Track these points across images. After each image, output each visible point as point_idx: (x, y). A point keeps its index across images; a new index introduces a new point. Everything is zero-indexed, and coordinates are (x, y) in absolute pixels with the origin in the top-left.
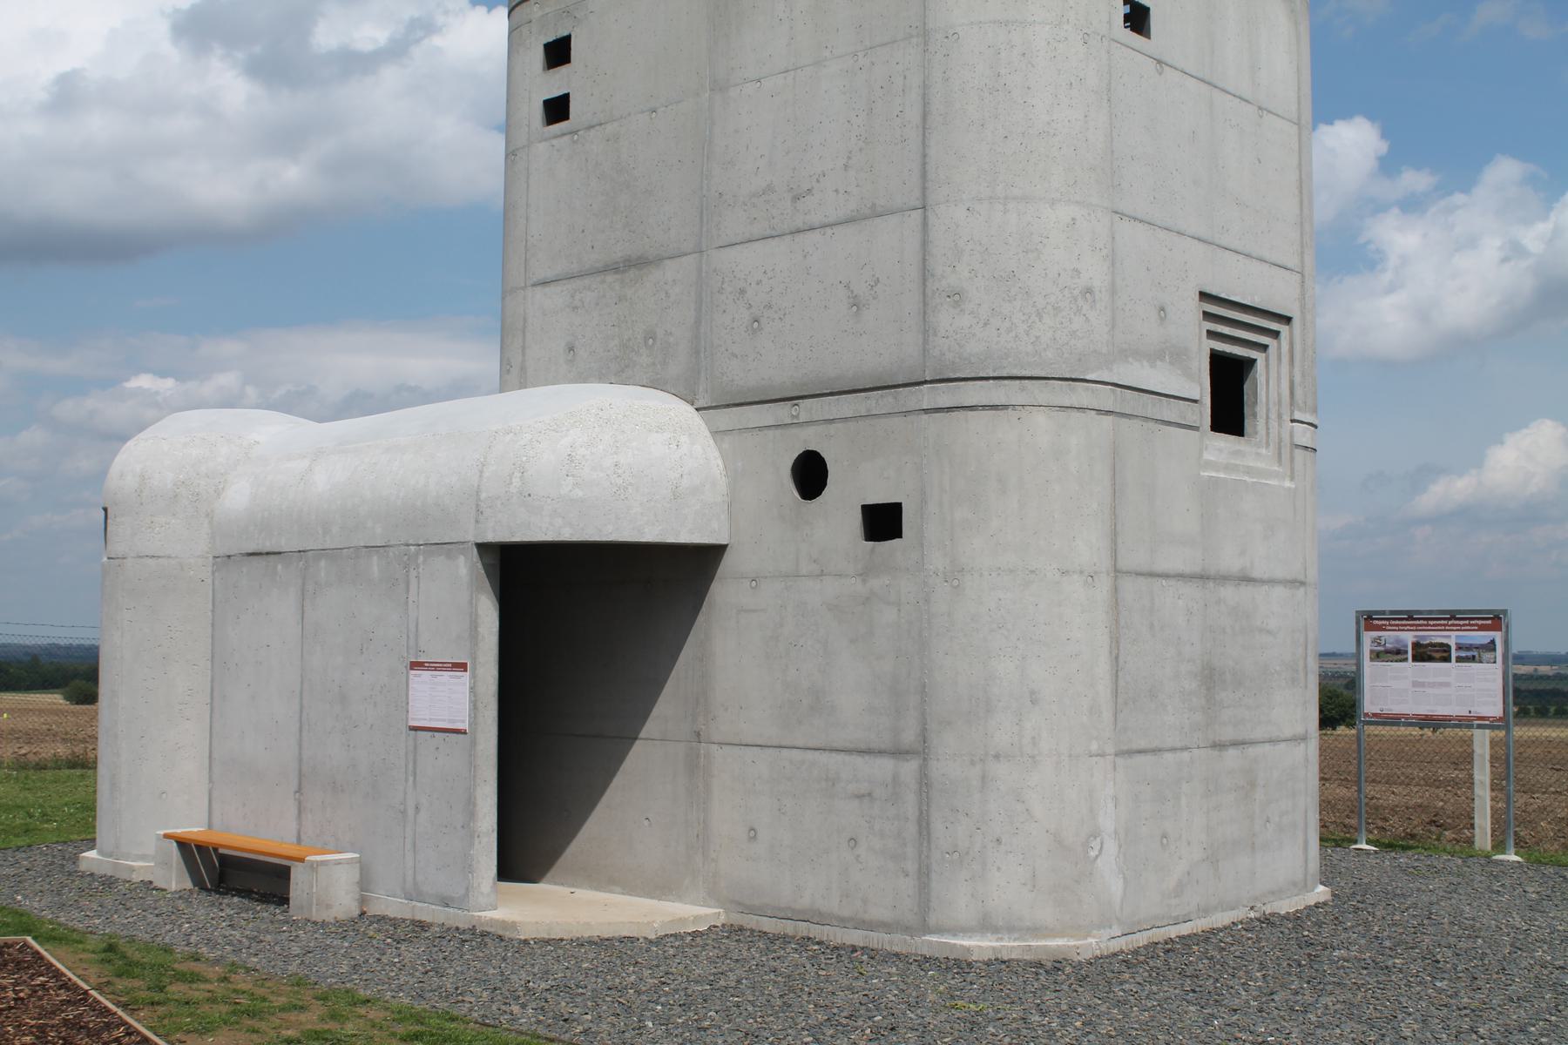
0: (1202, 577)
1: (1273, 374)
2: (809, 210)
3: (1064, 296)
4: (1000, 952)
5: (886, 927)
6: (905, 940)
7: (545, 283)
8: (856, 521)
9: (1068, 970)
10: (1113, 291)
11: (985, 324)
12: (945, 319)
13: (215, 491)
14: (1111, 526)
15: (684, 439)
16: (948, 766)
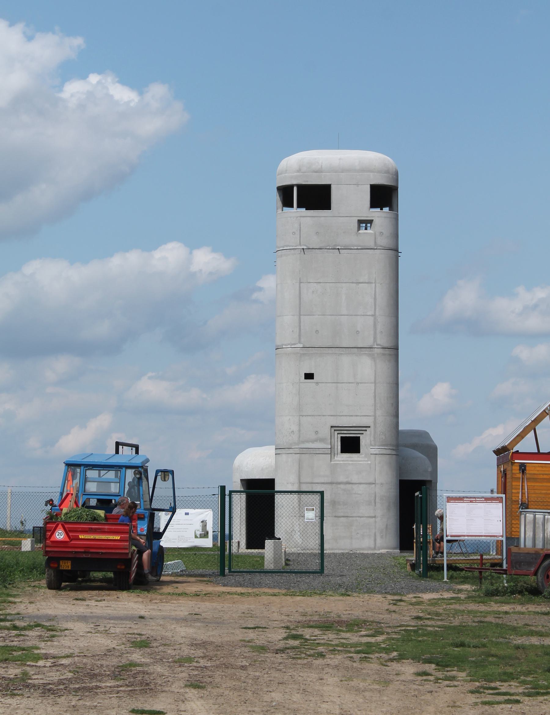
0: (331, 483)
10: (299, 431)
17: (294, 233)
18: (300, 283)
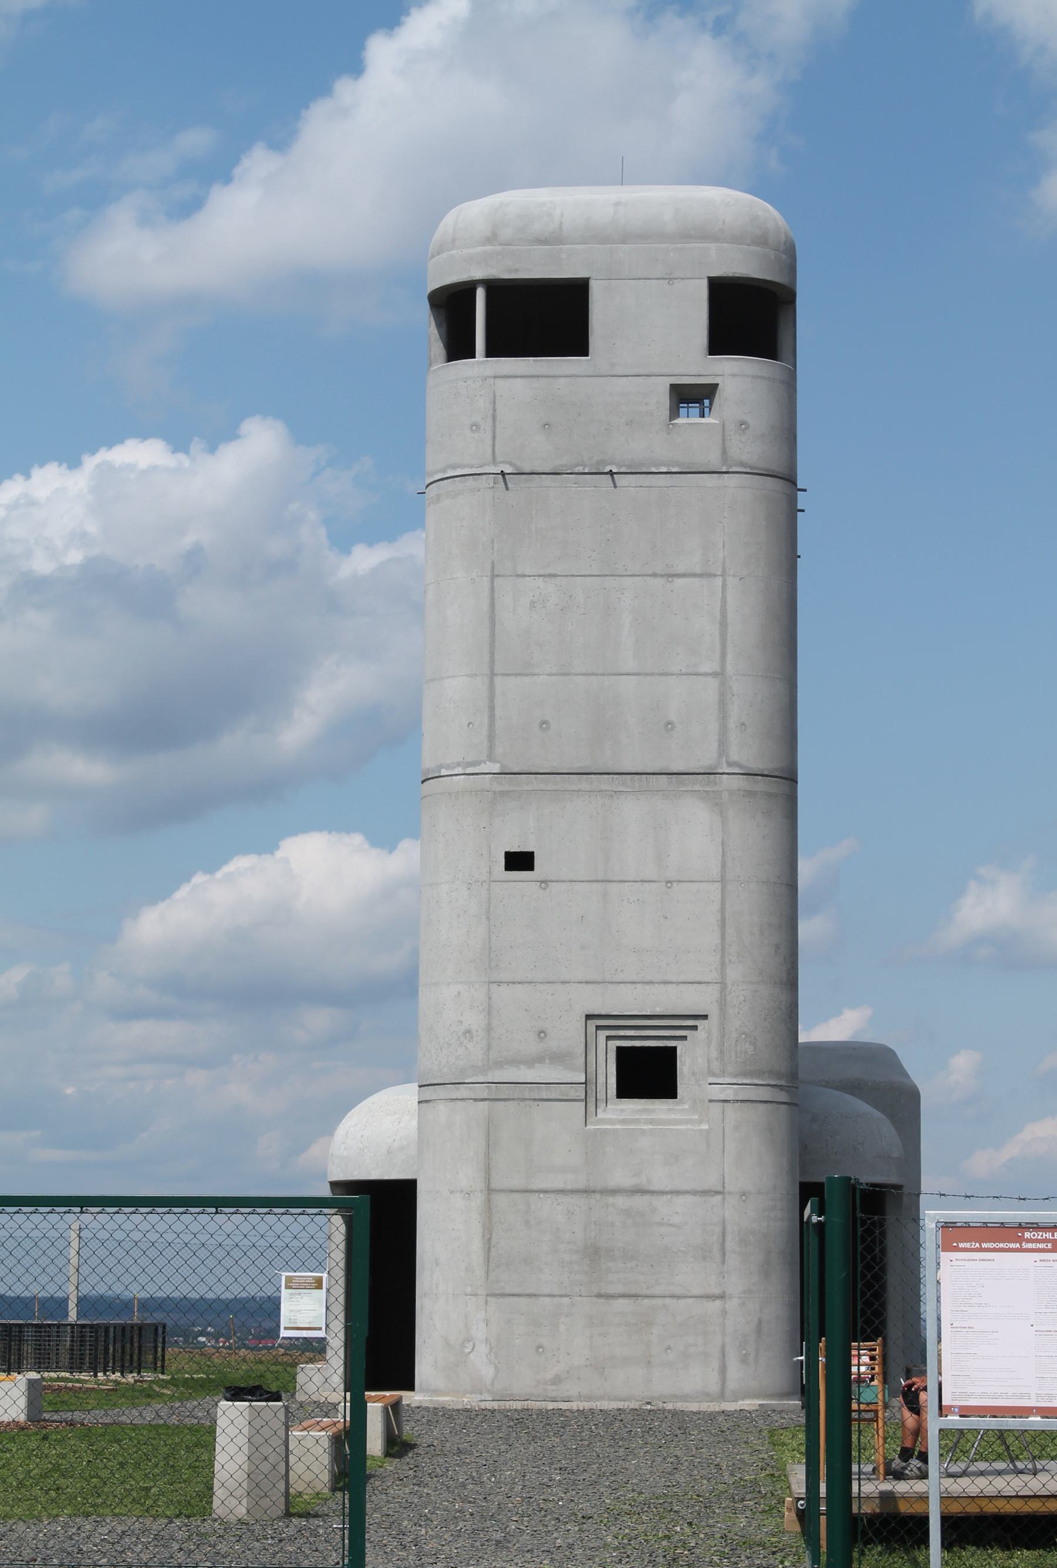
0: (587, 1192)
10: (489, 1029)
18: (494, 576)
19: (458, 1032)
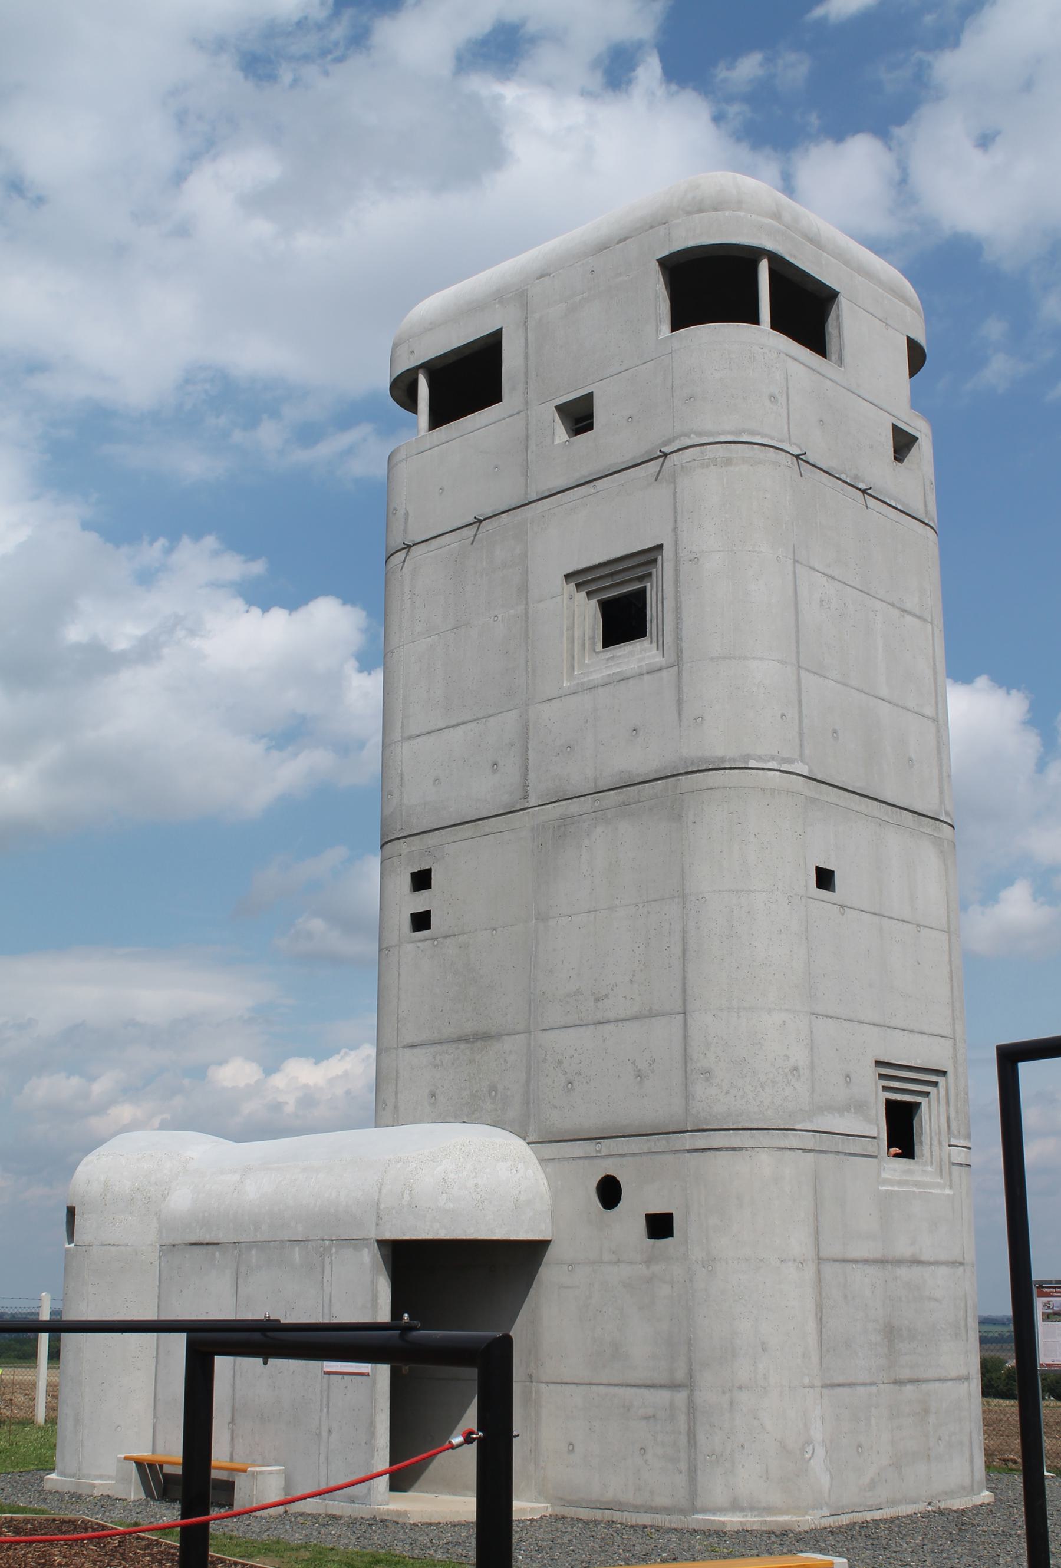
0: (882, 1262)
1: (934, 1112)
2: (607, 1009)
3: (778, 1073)
4: (746, 1525)
5: (667, 1510)
6: (681, 1519)
7: (412, 1046)
8: (642, 1224)
9: (791, 1535)
10: (812, 1067)
11: (727, 1093)
12: (700, 1089)
13: (162, 1196)
14: (814, 1228)
15: (520, 1166)
16: (707, 1395)
17: (773, 398)
19: (785, 1068)
